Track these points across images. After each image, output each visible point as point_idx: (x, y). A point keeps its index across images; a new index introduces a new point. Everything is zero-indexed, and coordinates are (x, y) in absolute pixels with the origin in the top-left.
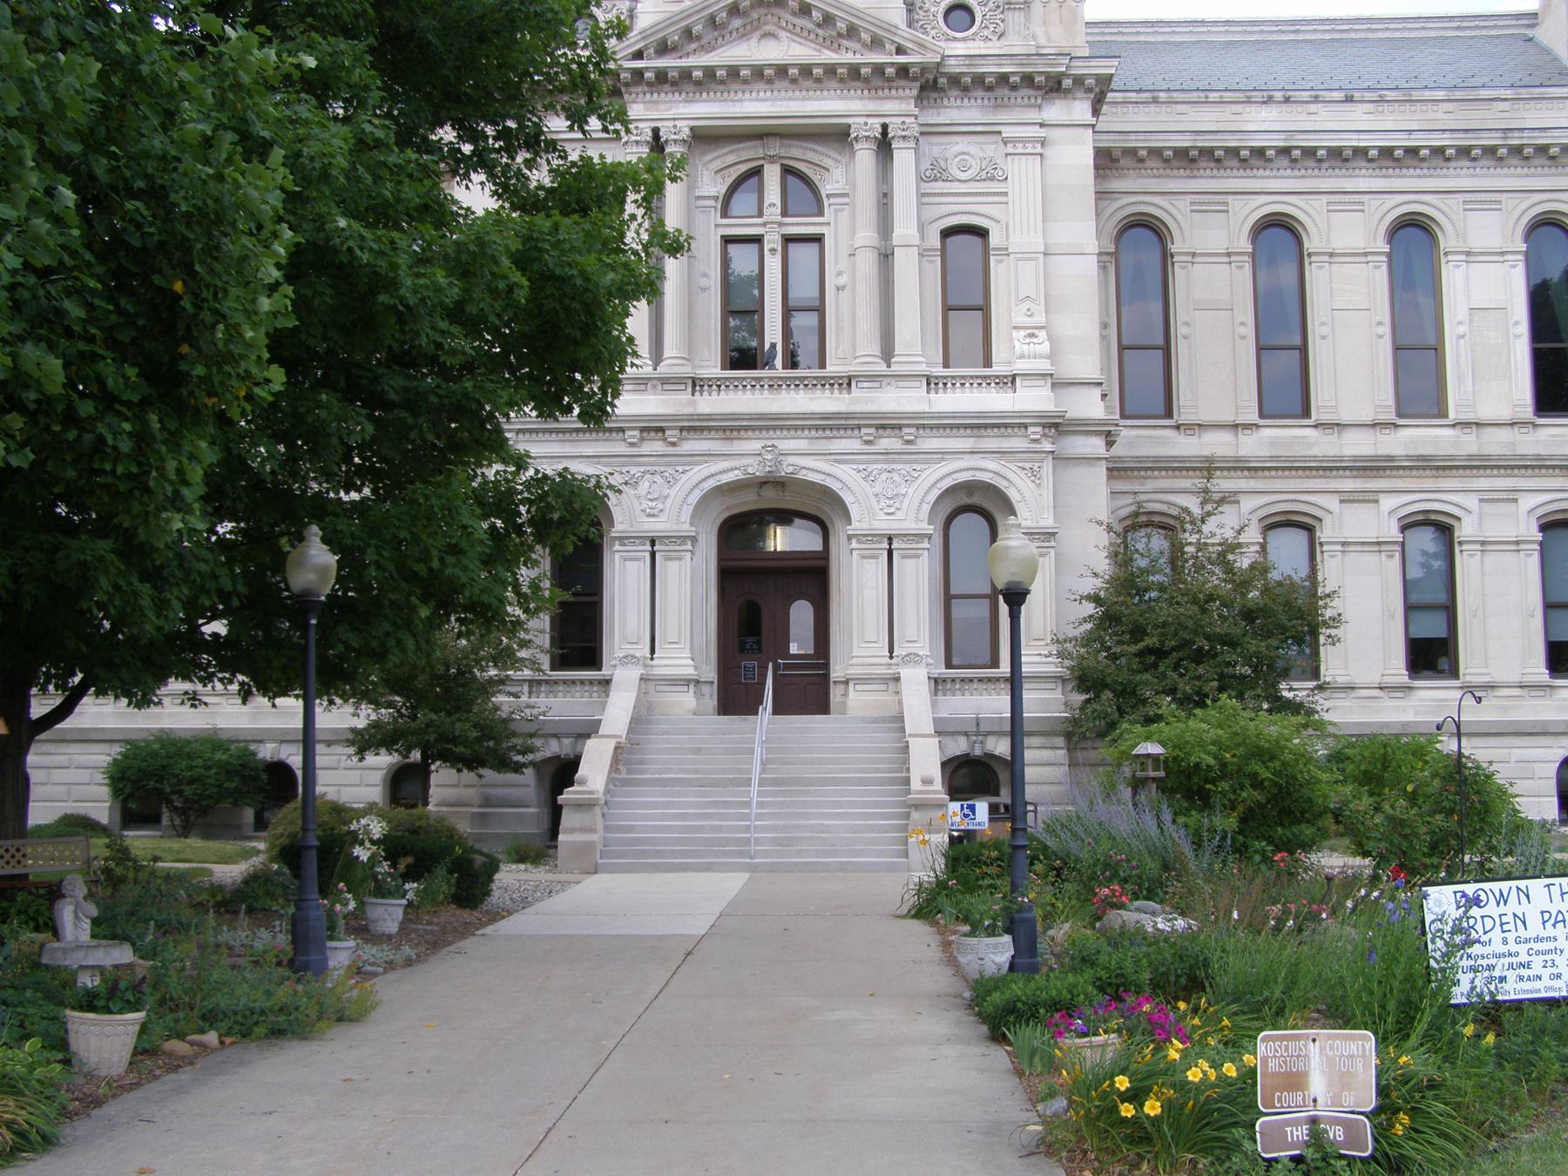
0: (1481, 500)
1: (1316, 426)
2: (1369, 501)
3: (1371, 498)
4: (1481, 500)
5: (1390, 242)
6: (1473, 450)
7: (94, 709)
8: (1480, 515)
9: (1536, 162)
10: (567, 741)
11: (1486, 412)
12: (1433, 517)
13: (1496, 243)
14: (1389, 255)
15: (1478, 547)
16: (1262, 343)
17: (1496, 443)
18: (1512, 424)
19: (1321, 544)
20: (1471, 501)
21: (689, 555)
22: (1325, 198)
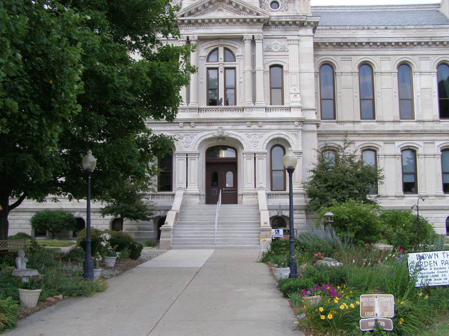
0: (424, 143)
1: (377, 122)
2: (392, 143)
3: (392, 142)
4: (424, 143)
5: (398, 69)
6: (422, 129)
7: (27, 203)
8: (424, 147)
9: (440, 46)
10: (162, 212)
11: (426, 118)
12: (410, 148)
13: (428, 69)
14: (398, 73)
15: (423, 156)
16: (361, 98)
17: (428, 126)
18: (433, 121)
19: (378, 155)
20: (421, 143)
21: (197, 158)
22: (379, 57)
